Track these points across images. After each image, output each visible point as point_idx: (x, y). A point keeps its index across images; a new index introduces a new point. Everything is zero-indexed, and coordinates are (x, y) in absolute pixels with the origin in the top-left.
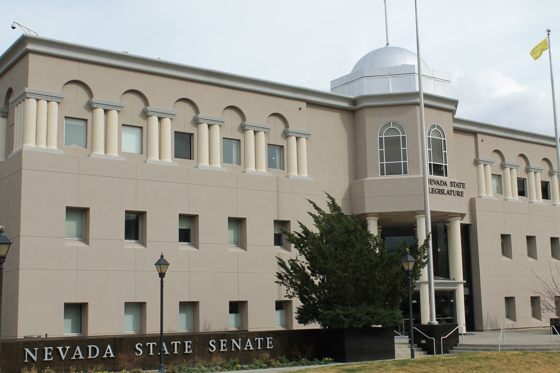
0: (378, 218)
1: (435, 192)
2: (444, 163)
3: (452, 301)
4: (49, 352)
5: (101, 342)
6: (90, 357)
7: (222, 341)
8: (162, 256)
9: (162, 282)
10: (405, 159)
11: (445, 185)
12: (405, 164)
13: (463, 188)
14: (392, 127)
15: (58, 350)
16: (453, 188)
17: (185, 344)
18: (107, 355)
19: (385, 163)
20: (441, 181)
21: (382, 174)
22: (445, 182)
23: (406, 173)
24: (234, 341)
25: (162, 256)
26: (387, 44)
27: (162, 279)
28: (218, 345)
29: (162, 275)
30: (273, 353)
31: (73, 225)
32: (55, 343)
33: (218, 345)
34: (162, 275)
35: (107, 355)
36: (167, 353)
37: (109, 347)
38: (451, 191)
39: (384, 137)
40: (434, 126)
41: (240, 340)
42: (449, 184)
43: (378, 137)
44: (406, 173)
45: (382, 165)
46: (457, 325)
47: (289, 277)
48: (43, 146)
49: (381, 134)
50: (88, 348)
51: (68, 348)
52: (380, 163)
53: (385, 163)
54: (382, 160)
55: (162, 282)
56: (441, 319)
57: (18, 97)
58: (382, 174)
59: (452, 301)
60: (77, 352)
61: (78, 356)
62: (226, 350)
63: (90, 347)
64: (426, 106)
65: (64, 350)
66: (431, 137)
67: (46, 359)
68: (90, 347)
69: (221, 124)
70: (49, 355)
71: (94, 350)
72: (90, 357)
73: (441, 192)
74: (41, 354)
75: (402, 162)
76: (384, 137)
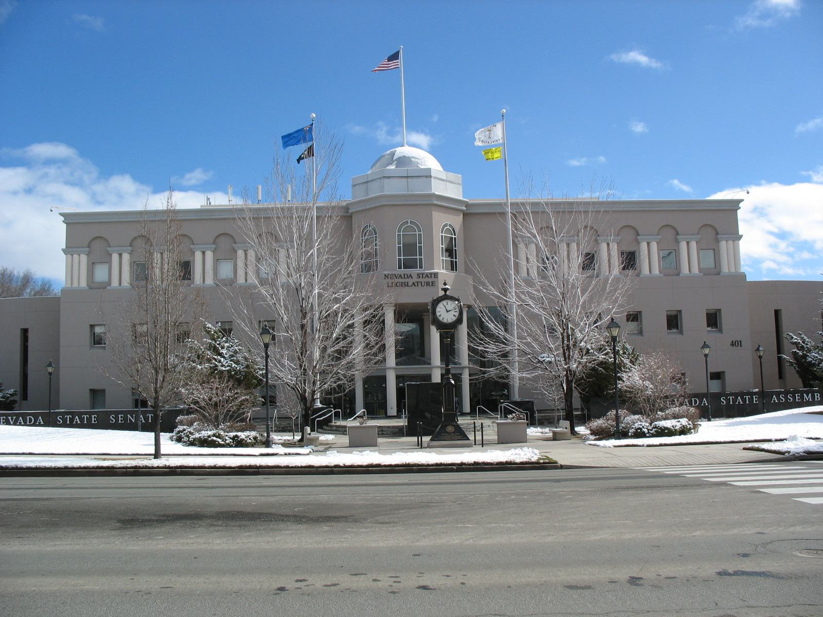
2: (445, 257)
3: (384, 385)
4: (94, 418)
7: (93, 416)
8: (705, 342)
9: (706, 360)
11: (410, 278)
14: (409, 225)
16: (421, 280)
18: (19, 423)
19: (402, 257)
21: (400, 268)
22: (410, 275)
24: (805, 395)
25: (705, 342)
27: (706, 358)
35: (19, 423)
37: (40, 418)
40: (446, 225)
42: (415, 276)
43: (397, 233)
51: (14, 417)
52: (398, 258)
53: (418, 257)
54: (400, 255)
56: (405, 399)
59: (384, 385)
62: (123, 422)
63: (28, 418)
65: (12, 419)
66: (443, 234)
67: (120, 422)
70: (121, 420)
73: (407, 285)
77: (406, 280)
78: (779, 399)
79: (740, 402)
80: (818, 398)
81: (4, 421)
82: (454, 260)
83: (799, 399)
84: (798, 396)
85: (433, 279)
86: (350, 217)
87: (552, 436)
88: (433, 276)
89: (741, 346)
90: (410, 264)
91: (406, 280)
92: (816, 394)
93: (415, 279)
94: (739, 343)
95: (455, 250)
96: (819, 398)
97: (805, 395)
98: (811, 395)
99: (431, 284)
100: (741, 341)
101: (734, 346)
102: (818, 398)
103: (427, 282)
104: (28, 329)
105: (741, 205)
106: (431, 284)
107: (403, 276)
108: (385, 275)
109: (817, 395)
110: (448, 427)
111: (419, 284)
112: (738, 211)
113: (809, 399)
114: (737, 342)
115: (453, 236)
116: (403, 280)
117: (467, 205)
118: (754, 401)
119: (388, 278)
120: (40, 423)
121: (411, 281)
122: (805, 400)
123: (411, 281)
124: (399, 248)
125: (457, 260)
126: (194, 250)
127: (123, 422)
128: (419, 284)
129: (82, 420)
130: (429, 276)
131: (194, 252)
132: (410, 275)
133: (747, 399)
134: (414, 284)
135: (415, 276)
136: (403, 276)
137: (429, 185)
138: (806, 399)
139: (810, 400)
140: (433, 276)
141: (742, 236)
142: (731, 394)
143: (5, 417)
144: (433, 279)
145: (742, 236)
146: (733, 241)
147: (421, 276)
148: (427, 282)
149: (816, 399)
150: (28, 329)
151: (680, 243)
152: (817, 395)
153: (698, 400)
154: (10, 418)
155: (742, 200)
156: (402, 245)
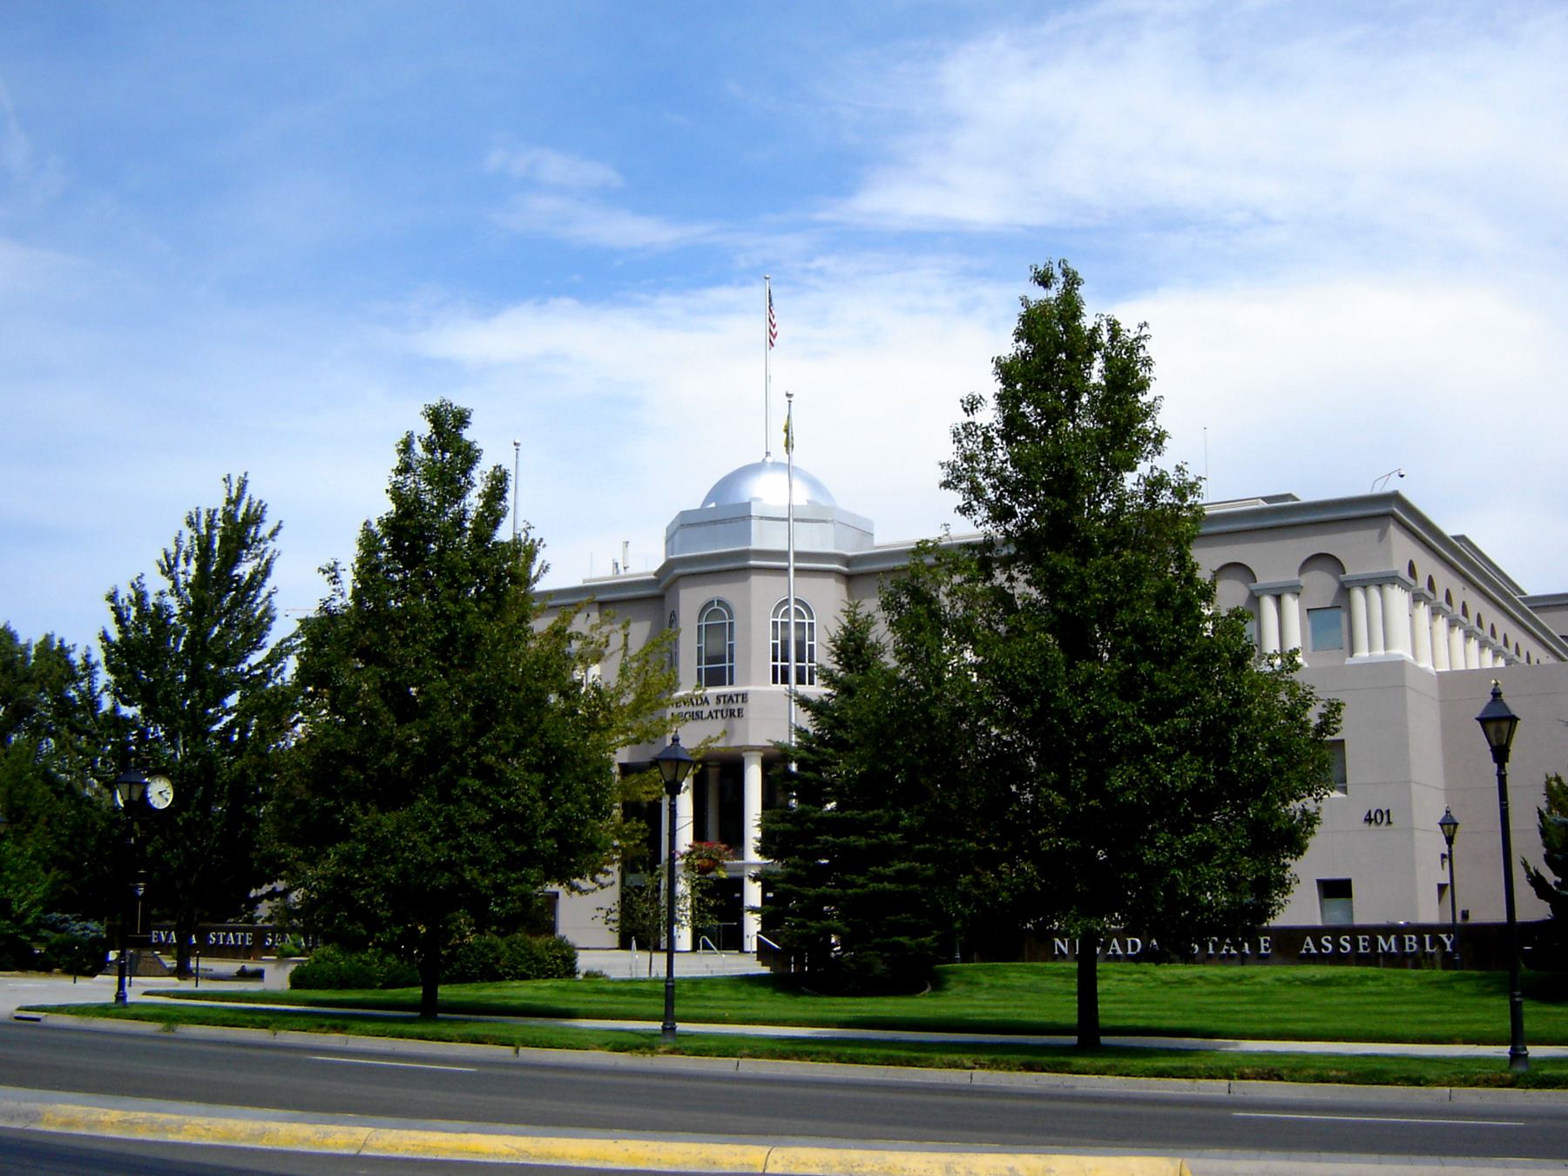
0: (761, 754)
5: (1372, 931)
6: (1130, 952)
7: (1360, 938)
14: (716, 607)
18: (1306, 950)
21: (775, 681)
23: (731, 683)
24: (1380, 938)
26: (768, 454)
28: (1355, 944)
30: (1448, 962)
32: (1419, 930)
35: (1306, 950)
36: (1211, 952)
38: (716, 711)
42: (712, 701)
46: (718, 949)
47: (1005, 849)
48: (1380, 652)
49: (775, 614)
50: (1127, 942)
57: (705, 520)
60: (1308, 945)
61: (1114, 951)
63: (1129, 940)
64: (797, 570)
68: (1129, 940)
69: (1296, 590)
70: (1265, 947)
72: (1130, 952)
75: (727, 664)
77: (699, 709)
78: (1319, 946)
80: (1411, 947)
81: (1267, 945)
82: (779, 664)
84: (1266, 941)
85: (740, 705)
87: (420, 997)
89: (1389, 822)
91: (699, 709)
92: (1406, 937)
93: (713, 706)
94: (1385, 817)
95: (811, 647)
96: (1415, 946)
97: (1380, 938)
98: (1396, 939)
99: (736, 714)
100: (1388, 812)
101: (1373, 823)
102: (1411, 947)
106: (736, 714)
109: (1411, 940)
111: (719, 715)
113: (1390, 948)
114: (1379, 821)
116: (695, 709)
117: (847, 561)
118: (1262, 948)
121: (706, 710)
122: (1380, 951)
123: (706, 710)
124: (775, 646)
125: (772, 663)
126: (1347, 586)
127: (1368, 951)
128: (719, 715)
129: (1437, 941)
131: (1349, 590)
133: (1130, 947)
135: (712, 701)
137: (747, 537)
138: (1382, 948)
139: (1394, 950)
140: (740, 699)
143: (1367, 937)
144: (740, 705)
146: (1380, 586)
147: (722, 699)
149: (1407, 950)
152: (1411, 940)
153: (1138, 940)
156: (779, 642)
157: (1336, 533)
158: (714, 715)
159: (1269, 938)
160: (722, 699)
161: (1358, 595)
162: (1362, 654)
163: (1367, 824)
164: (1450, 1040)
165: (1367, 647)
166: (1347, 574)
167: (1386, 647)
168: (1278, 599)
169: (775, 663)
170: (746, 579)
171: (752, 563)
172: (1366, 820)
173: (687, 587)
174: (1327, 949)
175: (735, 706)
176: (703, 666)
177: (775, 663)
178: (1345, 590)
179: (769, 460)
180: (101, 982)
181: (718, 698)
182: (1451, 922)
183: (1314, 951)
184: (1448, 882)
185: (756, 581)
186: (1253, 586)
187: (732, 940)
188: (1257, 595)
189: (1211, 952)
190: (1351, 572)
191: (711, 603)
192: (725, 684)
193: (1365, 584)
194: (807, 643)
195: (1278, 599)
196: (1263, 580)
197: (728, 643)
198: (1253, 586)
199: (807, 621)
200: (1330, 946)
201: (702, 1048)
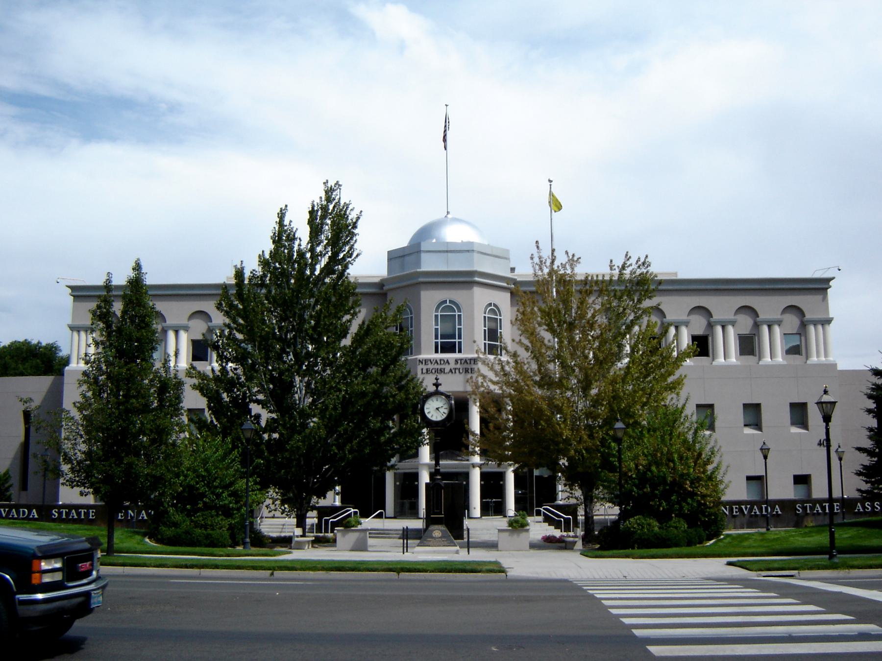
1: (432, 372)
3: (501, 483)
7: (91, 511)
9: (841, 464)
10: (460, 337)
12: (460, 343)
13: (425, 364)
15: (742, 508)
17: (733, 508)
20: (441, 360)
21: (436, 352)
22: (447, 360)
23: (460, 351)
26: (448, 213)
29: (765, 457)
31: (25, 397)
33: (761, 509)
34: (765, 457)
39: (439, 314)
40: (490, 304)
41: (728, 507)
44: (460, 351)
45: (436, 344)
48: (823, 359)
49: (437, 310)
53: (457, 340)
55: (841, 464)
58: (436, 352)
59: (501, 483)
61: (755, 513)
63: (21, 510)
65: (5, 511)
68: (21, 510)
69: (733, 323)
71: (24, 512)
74: (731, 510)
76: (439, 314)
79: (859, 510)
83: (93, 516)
86: (384, 295)
88: (472, 362)
90: (448, 348)
91: (442, 367)
93: (453, 365)
103: (466, 369)
104: (697, 405)
105: (831, 283)
106: (470, 371)
107: (439, 362)
108: (419, 360)
110: (434, 532)
111: (457, 371)
112: (828, 290)
115: (499, 317)
116: (439, 367)
118: (734, 512)
119: (422, 363)
120: (13, 516)
121: (447, 368)
123: (447, 368)
124: (485, 330)
127: (839, 511)
128: (457, 371)
130: (468, 361)
131: (805, 325)
132: (447, 360)
134: (451, 370)
135: (452, 363)
136: (439, 362)
137: (418, 263)
140: (472, 362)
141: (832, 319)
142: (64, 506)
145: (832, 319)
146: (822, 325)
147: (459, 362)
148: (466, 369)
150: (697, 405)
151: (807, 326)
153: (26, 510)
154: (743, 507)
155: (833, 278)
157: (726, 295)
158: (453, 371)
159: (94, 511)
160: (459, 362)
161: (812, 328)
162: (814, 359)
163: (819, 447)
164: (254, 556)
165: (769, 357)
166: (213, 322)
167: (826, 355)
168: (177, 332)
169: (436, 341)
170: (471, 288)
171: (477, 279)
172: (818, 444)
173: (427, 289)
174: (868, 509)
175: (469, 366)
176: (439, 340)
177: (436, 341)
178: (804, 325)
179: (449, 216)
180: (699, 547)
181: (456, 361)
182: (841, 495)
183: (861, 510)
184: (764, 474)
185: (477, 290)
186: (210, 324)
187: (413, 512)
188: (165, 329)
189: (808, 512)
190: (808, 316)
191: (445, 302)
192: (456, 352)
193: (815, 323)
194: (499, 331)
195: (177, 332)
196: (762, 316)
197: (457, 327)
198: (210, 324)
199: (457, 313)
200: (56, 514)
201: (278, 580)
